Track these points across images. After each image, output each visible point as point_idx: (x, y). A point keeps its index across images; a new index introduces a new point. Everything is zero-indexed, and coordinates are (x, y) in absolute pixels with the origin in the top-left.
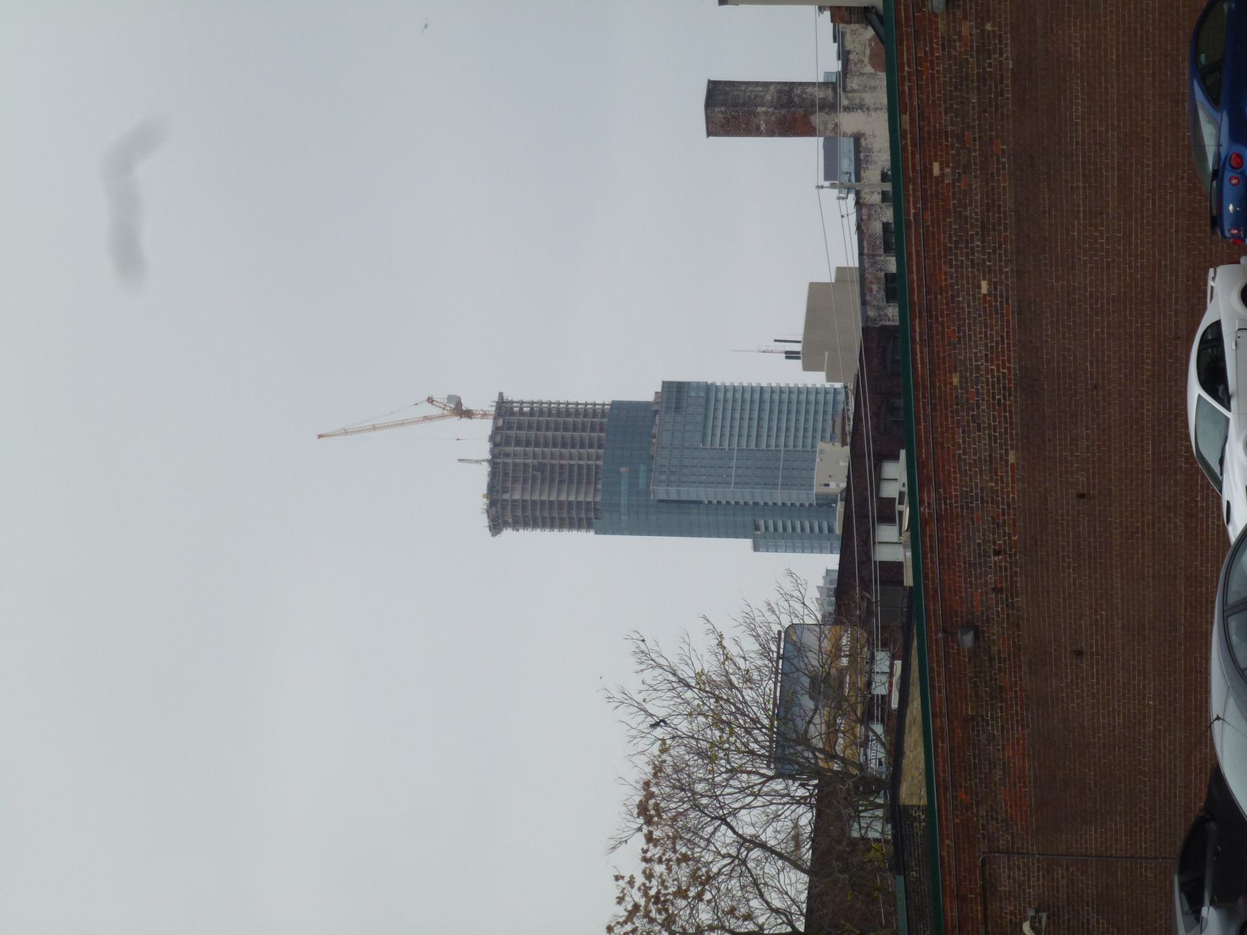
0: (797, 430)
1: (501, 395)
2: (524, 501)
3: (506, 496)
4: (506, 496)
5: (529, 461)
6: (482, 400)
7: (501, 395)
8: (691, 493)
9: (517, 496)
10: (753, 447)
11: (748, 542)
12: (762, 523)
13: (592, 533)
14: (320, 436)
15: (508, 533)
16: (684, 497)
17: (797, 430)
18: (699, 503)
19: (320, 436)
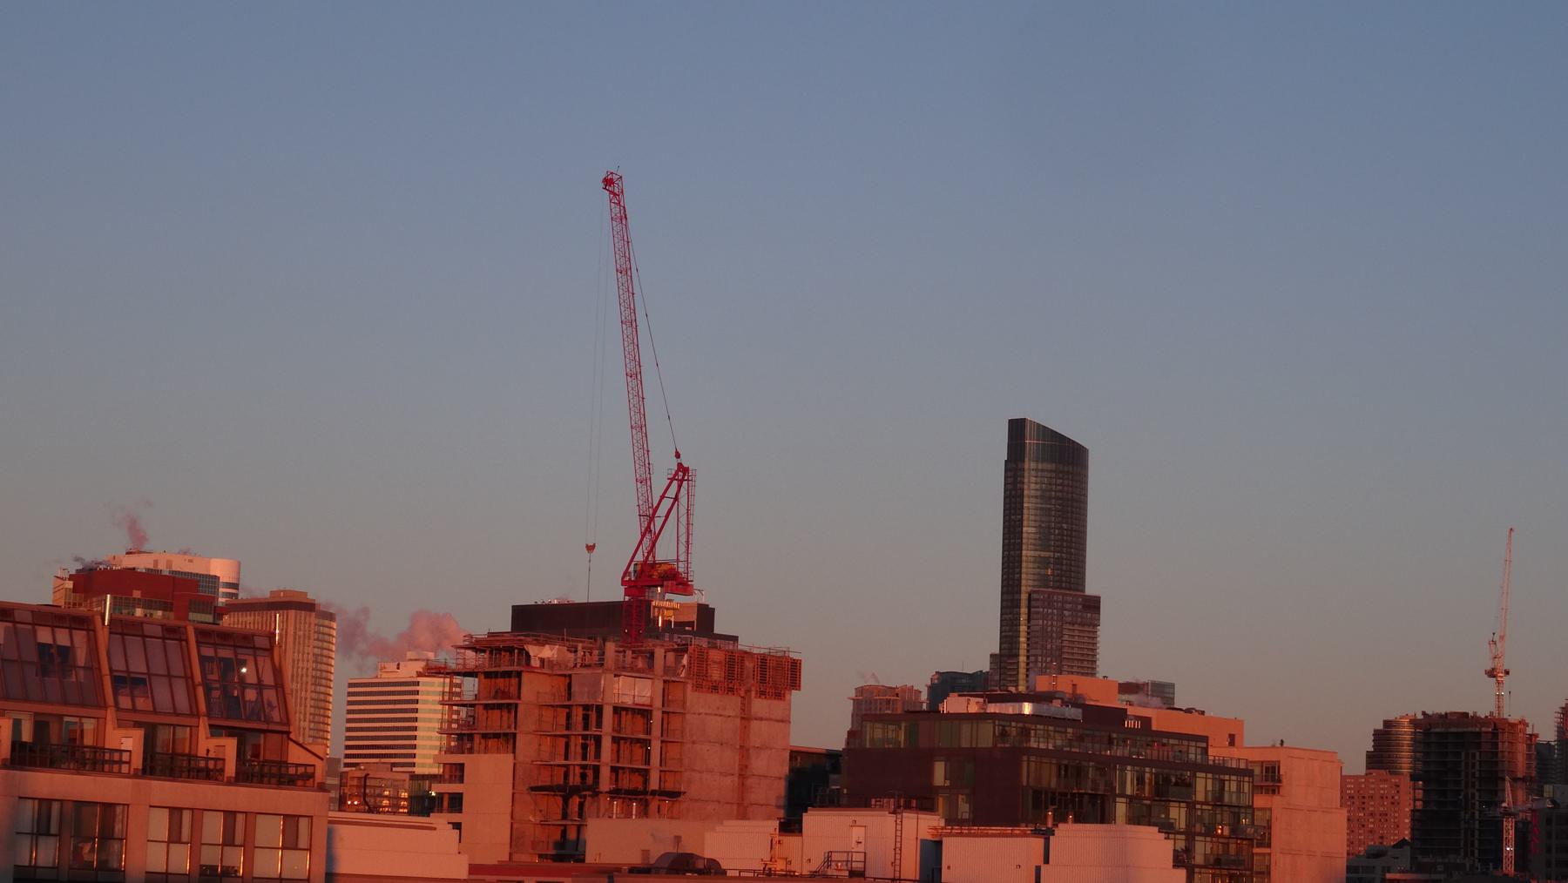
11: (997, 651)
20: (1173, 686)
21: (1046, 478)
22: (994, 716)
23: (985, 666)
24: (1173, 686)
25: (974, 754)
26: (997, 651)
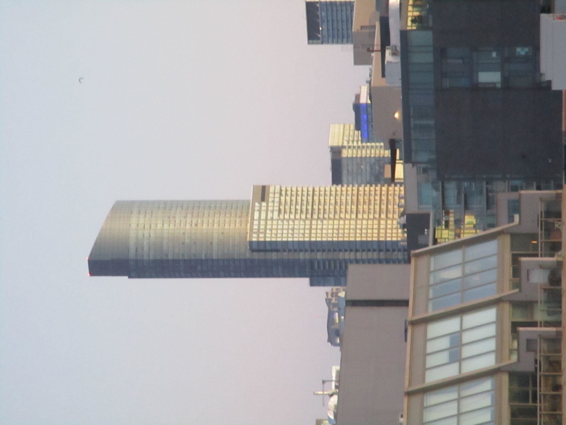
11: (306, 280)
22: (404, 34)
23: (321, 292)
25: (441, 52)
26: (306, 280)
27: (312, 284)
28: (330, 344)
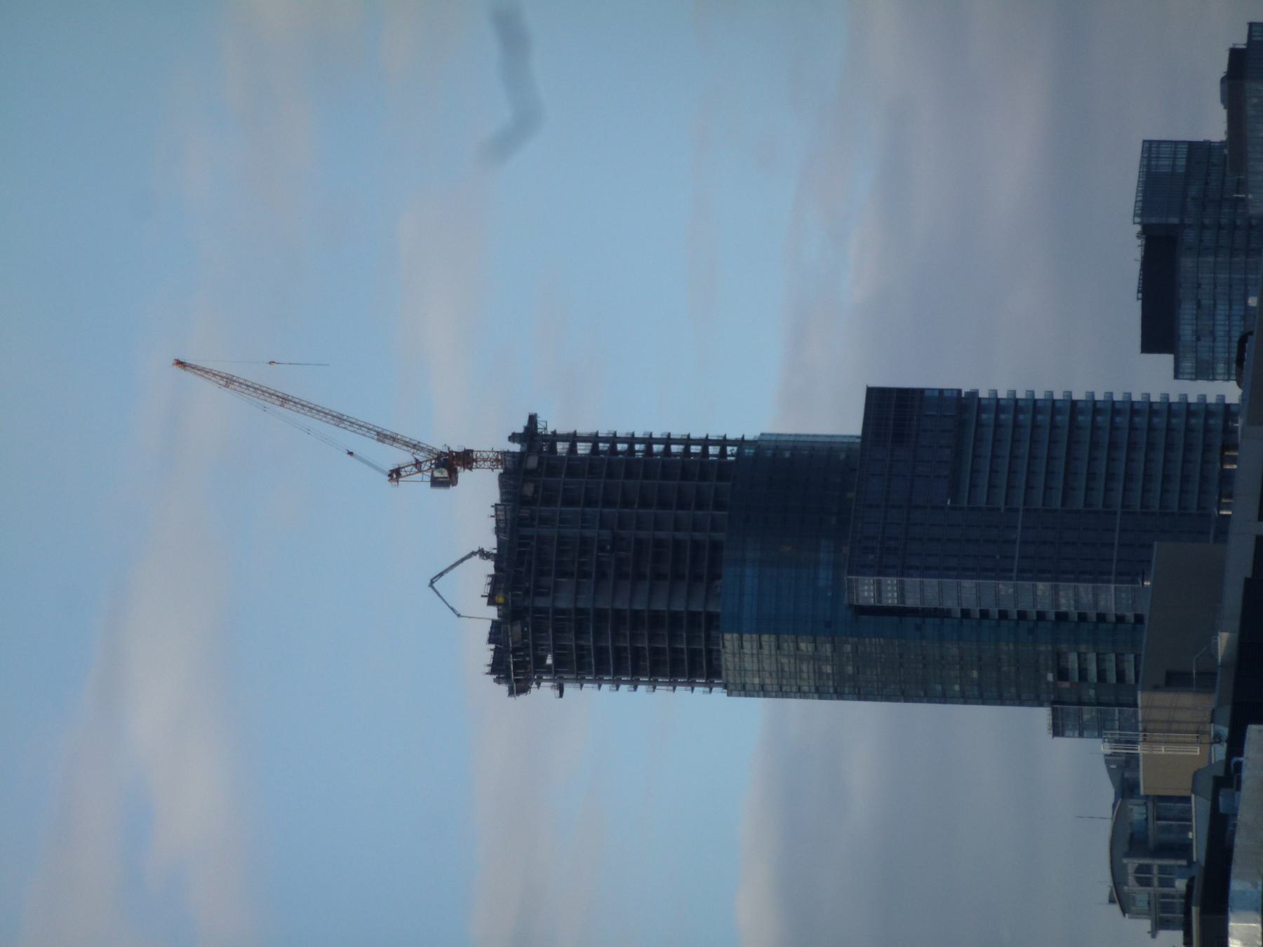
0: (1147, 477)
1: (533, 419)
2: (579, 611)
3: (542, 602)
4: (542, 602)
5: (590, 533)
6: (493, 435)
7: (533, 419)
8: (922, 591)
9: (564, 602)
10: (1057, 503)
11: (1042, 716)
12: (1072, 661)
13: (719, 694)
14: (180, 363)
15: (543, 692)
16: (911, 602)
17: (1147, 477)
18: (940, 614)
19: (180, 363)
20: (1151, 149)
21: (620, 560)
24: (1151, 149)
26: (1042, 716)
27: (1058, 730)
28: (1116, 908)
